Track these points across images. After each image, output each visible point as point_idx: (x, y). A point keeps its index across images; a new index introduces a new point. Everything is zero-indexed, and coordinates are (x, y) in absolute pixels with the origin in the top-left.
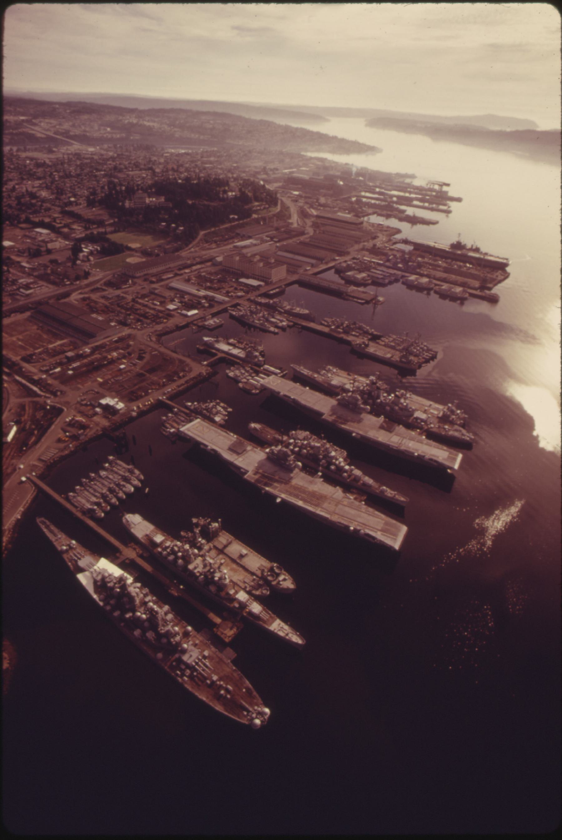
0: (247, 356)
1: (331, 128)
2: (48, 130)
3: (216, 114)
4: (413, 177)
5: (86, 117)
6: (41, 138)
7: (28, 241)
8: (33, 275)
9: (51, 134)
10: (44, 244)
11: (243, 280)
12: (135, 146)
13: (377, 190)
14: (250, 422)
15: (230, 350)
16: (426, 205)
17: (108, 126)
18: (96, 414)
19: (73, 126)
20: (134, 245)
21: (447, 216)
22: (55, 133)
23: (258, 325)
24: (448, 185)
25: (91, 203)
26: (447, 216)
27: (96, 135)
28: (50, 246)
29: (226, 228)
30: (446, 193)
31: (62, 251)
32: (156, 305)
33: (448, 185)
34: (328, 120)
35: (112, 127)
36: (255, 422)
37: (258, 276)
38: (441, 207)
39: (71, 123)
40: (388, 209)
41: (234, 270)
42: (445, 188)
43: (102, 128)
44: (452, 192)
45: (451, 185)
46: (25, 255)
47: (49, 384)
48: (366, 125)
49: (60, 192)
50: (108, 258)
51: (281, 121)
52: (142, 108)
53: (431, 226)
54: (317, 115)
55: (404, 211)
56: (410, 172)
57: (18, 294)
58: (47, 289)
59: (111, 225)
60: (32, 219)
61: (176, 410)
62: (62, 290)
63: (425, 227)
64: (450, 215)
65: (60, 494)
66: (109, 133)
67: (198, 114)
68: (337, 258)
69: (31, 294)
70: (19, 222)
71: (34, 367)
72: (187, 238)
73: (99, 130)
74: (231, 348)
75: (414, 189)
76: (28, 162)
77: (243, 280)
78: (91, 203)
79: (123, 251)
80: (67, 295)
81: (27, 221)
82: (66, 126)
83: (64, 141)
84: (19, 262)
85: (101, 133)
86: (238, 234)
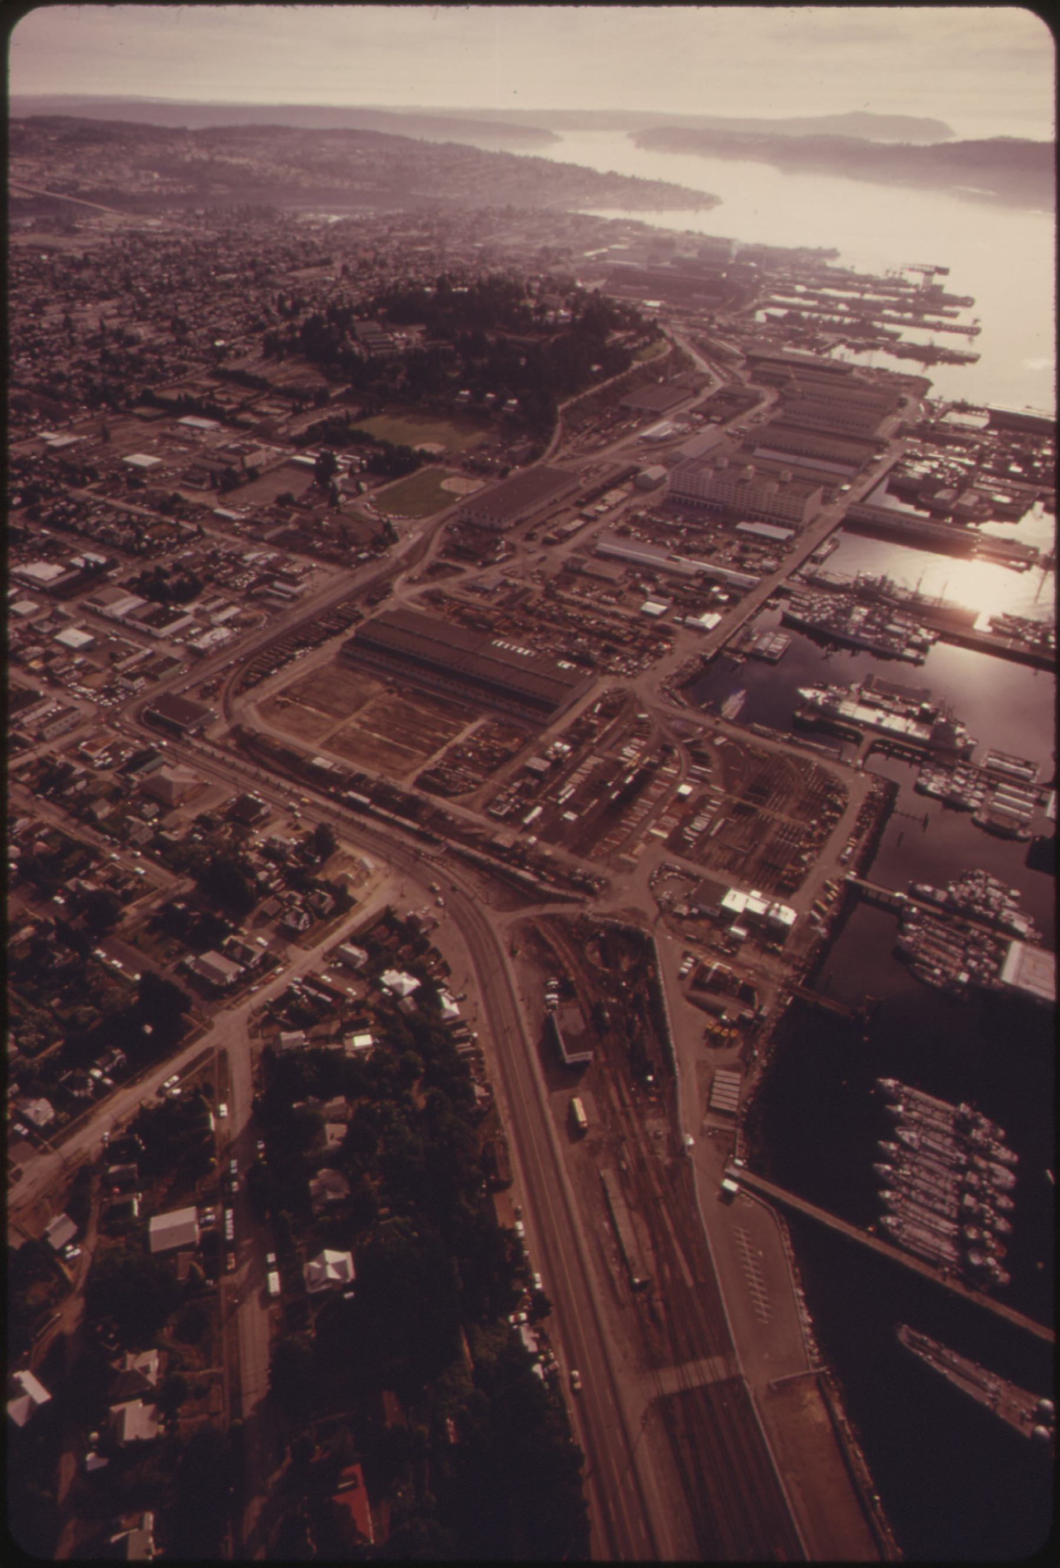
0: (934, 735)
1: (566, 150)
2: (30, 182)
3: (350, 134)
4: (833, 254)
5: (95, 149)
6: (25, 200)
7: (182, 449)
8: (262, 540)
9: (40, 190)
10: (237, 458)
11: (742, 526)
12: (235, 210)
13: (800, 289)
14: (154, 1514)
15: (880, 720)
16: (908, 315)
17: (154, 170)
18: (735, 942)
19: (77, 170)
20: (434, 448)
21: (970, 340)
22: (48, 189)
23: (870, 643)
24: (943, 271)
25: (273, 349)
26: (970, 340)
27: (134, 189)
28: (250, 460)
29: (596, 396)
30: (939, 288)
31: (277, 469)
32: (609, 604)
33: (943, 271)
34: (558, 139)
35: (164, 172)
36: (156, 1520)
37: (766, 513)
38: (947, 321)
39: (72, 166)
40: (864, 331)
41: (702, 502)
42: (937, 279)
43: (143, 172)
44: (950, 286)
45: (951, 273)
46: (204, 486)
47: (546, 859)
48: (638, 145)
49: (179, 327)
50: (394, 483)
51: (490, 145)
52: (193, 125)
53: (968, 365)
54: (540, 127)
55: (895, 336)
56: (826, 245)
57: (269, 595)
58: (326, 575)
59: (342, 399)
60: (157, 394)
61: (914, 910)
62: (365, 576)
63: (955, 368)
64: (976, 338)
65: (862, 1225)
66: (158, 183)
67: (310, 135)
68: (878, 457)
69: (302, 593)
70: (131, 404)
71: (465, 805)
72: (536, 424)
73: (137, 177)
74: (880, 714)
75: (861, 282)
76: (44, 257)
77: (742, 526)
78: (273, 349)
79: (418, 466)
80: (378, 590)
81: (147, 399)
82: (63, 172)
83: (77, 205)
84: (202, 507)
85: (143, 186)
86: (625, 409)
